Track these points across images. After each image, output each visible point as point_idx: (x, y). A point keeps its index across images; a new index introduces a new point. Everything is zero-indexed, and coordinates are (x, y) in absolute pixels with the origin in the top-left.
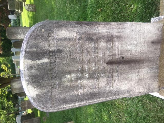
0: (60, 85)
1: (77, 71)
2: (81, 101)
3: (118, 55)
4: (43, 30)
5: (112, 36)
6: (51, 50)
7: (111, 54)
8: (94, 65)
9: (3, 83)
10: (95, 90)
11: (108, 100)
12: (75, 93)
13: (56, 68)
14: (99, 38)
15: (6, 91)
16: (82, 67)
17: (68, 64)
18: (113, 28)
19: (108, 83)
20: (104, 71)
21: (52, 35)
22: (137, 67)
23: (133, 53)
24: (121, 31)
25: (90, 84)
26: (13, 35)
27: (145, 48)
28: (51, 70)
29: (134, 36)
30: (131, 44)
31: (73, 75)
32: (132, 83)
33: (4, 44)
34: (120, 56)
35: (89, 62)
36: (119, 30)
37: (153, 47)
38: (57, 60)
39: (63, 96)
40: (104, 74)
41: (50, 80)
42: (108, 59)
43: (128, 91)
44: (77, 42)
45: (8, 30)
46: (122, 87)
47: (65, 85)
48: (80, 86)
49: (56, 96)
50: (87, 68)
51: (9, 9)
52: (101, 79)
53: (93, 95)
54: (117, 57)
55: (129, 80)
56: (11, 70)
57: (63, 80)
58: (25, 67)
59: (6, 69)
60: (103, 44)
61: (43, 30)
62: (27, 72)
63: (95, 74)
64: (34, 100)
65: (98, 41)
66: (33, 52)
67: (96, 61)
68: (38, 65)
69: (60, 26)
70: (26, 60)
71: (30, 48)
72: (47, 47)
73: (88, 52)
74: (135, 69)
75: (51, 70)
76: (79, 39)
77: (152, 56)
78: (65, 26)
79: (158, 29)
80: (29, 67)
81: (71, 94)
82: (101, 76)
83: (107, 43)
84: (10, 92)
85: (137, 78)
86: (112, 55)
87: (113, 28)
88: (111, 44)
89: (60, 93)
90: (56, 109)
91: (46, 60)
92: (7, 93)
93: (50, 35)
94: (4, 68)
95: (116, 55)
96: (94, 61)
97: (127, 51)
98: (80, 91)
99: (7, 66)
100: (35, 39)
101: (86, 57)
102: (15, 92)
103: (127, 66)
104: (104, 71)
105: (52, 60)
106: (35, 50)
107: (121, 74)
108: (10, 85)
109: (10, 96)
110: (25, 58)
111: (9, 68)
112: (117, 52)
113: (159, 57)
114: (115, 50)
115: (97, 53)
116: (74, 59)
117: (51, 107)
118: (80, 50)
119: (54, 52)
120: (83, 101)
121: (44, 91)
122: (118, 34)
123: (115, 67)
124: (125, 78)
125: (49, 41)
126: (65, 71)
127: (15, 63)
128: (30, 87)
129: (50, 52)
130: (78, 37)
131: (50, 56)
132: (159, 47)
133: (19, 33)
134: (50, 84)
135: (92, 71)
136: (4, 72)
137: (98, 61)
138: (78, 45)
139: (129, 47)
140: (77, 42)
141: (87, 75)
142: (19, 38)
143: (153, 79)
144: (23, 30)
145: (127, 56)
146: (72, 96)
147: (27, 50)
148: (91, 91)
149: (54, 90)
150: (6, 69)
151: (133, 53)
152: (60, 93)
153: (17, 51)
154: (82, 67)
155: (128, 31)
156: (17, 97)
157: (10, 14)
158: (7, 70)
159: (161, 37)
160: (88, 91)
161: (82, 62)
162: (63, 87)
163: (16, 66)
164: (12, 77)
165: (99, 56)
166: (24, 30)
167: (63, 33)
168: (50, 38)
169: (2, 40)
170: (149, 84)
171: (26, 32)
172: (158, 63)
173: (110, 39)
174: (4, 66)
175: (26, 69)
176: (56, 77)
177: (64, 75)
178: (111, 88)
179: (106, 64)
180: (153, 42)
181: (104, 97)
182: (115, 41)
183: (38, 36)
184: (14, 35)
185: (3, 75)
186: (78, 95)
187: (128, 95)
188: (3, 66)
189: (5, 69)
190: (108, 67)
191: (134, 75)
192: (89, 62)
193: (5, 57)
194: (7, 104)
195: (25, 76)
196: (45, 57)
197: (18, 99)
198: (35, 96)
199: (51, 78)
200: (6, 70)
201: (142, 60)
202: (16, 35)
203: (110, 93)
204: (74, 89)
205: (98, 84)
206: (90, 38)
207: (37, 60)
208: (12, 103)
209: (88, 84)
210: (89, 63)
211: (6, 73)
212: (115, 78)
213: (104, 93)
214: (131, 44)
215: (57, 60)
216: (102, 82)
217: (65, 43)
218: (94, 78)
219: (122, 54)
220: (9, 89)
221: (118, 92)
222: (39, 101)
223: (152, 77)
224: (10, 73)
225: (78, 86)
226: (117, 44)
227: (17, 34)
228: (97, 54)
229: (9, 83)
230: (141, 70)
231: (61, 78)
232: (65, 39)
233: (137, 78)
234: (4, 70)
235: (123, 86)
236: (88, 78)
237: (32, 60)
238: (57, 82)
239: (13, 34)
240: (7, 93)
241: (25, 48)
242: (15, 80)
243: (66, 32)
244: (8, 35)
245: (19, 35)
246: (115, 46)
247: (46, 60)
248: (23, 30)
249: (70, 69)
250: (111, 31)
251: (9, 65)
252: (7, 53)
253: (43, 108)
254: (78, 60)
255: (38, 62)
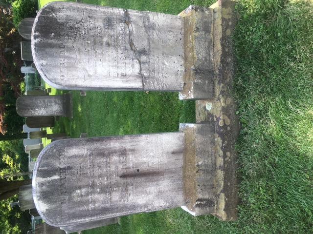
0: (69, 200)
1: (87, 186)
2: (92, 216)
3: (133, 168)
4: (55, 150)
5: (125, 150)
6: (61, 167)
7: (125, 167)
8: (106, 180)
9: (5, 191)
10: (108, 205)
11: (123, 215)
12: (86, 208)
13: (66, 184)
14: (111, 153)
15: (9, 206)
16: (93, 182)
17: (79, 180)
18: (127, 143)
19: (122, 197)
20: (117, 185)
21: (63, 153)
22: (156, 179)
23: (150, 165)
24: (135, 144)
25: (102, 199)
26: (27, 110)
27: (165, 160)
28: (61, 186)
29: (150, 148)
30: (147, 156)
31: (84, 190)
32: (151, 197)
33: (9, 116)
34: (135, 169)
35: (100, 176)
36: (133, 144)
37: (173, 158)
38: (67, 176)
39: (73, 211)
40: (117, 188)
41: (60, 195)
42: (121, 173)
43: (146, 206)
44: (88, 158)
45: (21, 101)
46: (138, 201)
47: (75, 200)
48: (90, 200)
49: (66, 212)
50: (98, 182)
51: (22, 59)
52: (114, 194)
53: (104, 210)
54: (132, 170)
55: (147, 193)
56: (19, 165)
57: (72, 195)
58: (36, 184)
59: (11, 164)
60: (115, 158)
61: (55, 150)
62: (38, 189)
63: (107, 188)
64: (44, 215)
65: (109, 155)
66: (45, 170)
67: (108, 175)
68: (49, 182)
69: (70, 146)
70: (38, 178)
71: (42, 167)
72: (57, 165)
73: (100, 167)
74: (153, 182)
75: (61, 186)
76: (90, 155)
77: (173, 166)
78: (76, 145)
79: (179, 138)
80: (40, 184)
81: (81, 209)
82: (114, 190)
83: (120, 157)
84: (16, 208)
85: (156, 191)
86: (126, 168)
87: (125, 142)
88: (125, 158)
89: (69, 208)
90: (66, 224)
91: (56, 177)
92: (10, 209)
93: (61, 154)
94: (7, 162)
95: (130, 168)
96: (106, 176)
97: (143, 163)
98: (91, 206)
99: (13, 156)
100: (47, 158)
101: (97, 171)
102: (26, 208)
103: (143, 179)
104: (117, 185)
105: (63, 177)
106: (46, 168)
107: (136, 187)
108: (18, 195)
109: (16, 215)
110: (37, 176)
111: (16, 162)
112: (131, 165)
113: (182, 167)
114: (129, 163)
115: (109, 167)
116: (85, 175)
117: (60, 222)
118: (91, 166)
119: (64, 169)
120: (94, 216)
121: (53, 206)
122: (133, 147)
123: (129, 180)
124: (142, 192)
125: (60, 159)
126: (76, 187)
127: (28, 152)
128: (40, 202)
129: (61, 169)
130: (89, 153)
131: (61, 173)
132: (181, 157)
133: (38, 107)
134: (60, 200)
135: (104, 185)
136: (7, 168)
137: (110, 175)
138: (88, 161)
139: (145, 159)
140: (88, 158)
141: (98, 190)
142: (37, 114)
143: (176, 192)
144: (44, 102)
145: (143, 168)
146: (82, 211)
147: (40, 169)
148: (103, 206)
149: (63, 205)
150: (11, 164)
151: (150, 165)
152: (69, 208)
153: (32, 131)
154: (93, 182)
155: (142, 144)
156: (30, 217)
157: (23, 66)
158: (13, 165)
159: (183, 146)
160: (99, 206)
161: (93, 177)
162: (73, 202)
163: (29, 157)
164: (21, 179)
165: (112, 169)
166: (46, 100)
167: (74, 151)
168: (61, 157)
169: (7, 109)
170: (171, 197)
171: (49, 104)
172: (181, 174)
173: (123, 153)
174: (8, 157)
175: (38, 185)
176: (66, 192)
177: (74, 191)
178: (126, 202)
179: (119, 178)
180: (173, 153)
181: (117, 212)
182: (129, 155)
183: (50, 155)
184: (28, 109)
185: (4, 176)
186: (88, 210)
187: (146, 209)
188: (7, 159)
189: (10, 163)
190: (122, 181)
191: (153, 188)
192: (100, 176)
193: (9, 139)
194: (9, 231)
195: (36, 192)
196: (55, 174)
197: (31, 221)
198: (45, 211)
199: (61, 193)
200: (11, 166)
201: (161, 172)
202: (32, 109)
203: (125, 207)
204: (84, 203)
205: (111, 199)
206: (101, 154)
207: (48, 178)
208: (19, 229)
209: (99, 199)
210: (101, 177)
211: (10, 171)
212: (129, 192)
213: (117, 208)
214: (147, 156)
215: (67, 176)
216: (116, 197)
217: (75, 160)
218: (106, 192)
219: (137, 167)
220: (14, 201)
221: (134, 207)
222: (48, 216)
223: (175, 189)
224: (18, 171)
225: (89, 200)
226: (131, 157)
227: (34, 107)
228: (109, 168)
229: (16, 190)
230: (160, 182)
231: (71, 193)
232: (76, 156)
233: (156, 191)
234: (8, 165)
235: (140, 200)
236: (99, 193)
237: (44, 177)
238: (67, 197)
239: (27, 107)
240: (10, 209)
241: (37, 167)
242: (26, 186)
243: (77, 150)
244: (19, 110)
245: (37, 109)
246: (129, 159)
247: (56, 177)
248: (44, 102)
249: (80, 184)
250: (123, 145)
251: (17, 156)
252: (15, 127)
253: (53, 223)
254: (89, 175)
255: (49, 179)
